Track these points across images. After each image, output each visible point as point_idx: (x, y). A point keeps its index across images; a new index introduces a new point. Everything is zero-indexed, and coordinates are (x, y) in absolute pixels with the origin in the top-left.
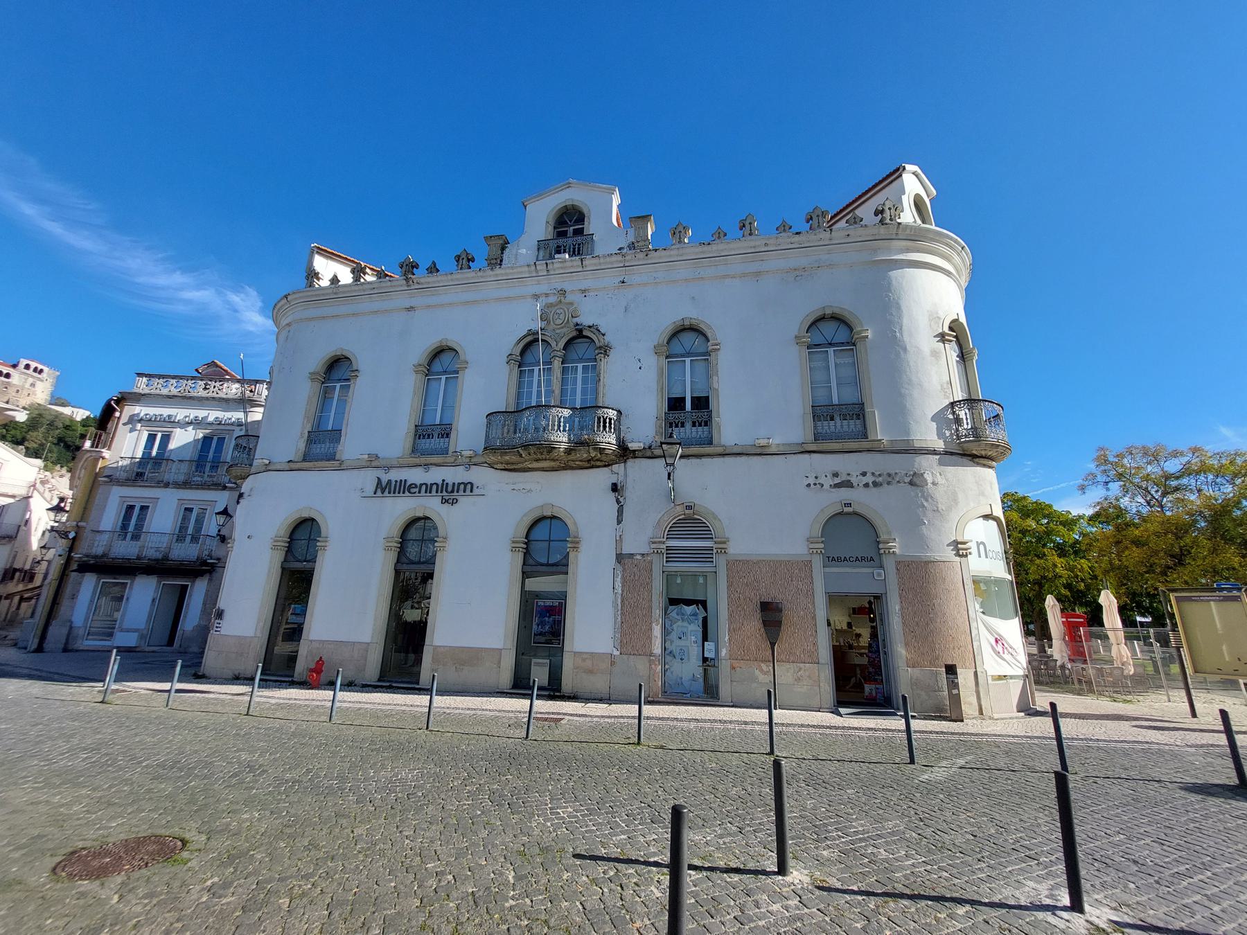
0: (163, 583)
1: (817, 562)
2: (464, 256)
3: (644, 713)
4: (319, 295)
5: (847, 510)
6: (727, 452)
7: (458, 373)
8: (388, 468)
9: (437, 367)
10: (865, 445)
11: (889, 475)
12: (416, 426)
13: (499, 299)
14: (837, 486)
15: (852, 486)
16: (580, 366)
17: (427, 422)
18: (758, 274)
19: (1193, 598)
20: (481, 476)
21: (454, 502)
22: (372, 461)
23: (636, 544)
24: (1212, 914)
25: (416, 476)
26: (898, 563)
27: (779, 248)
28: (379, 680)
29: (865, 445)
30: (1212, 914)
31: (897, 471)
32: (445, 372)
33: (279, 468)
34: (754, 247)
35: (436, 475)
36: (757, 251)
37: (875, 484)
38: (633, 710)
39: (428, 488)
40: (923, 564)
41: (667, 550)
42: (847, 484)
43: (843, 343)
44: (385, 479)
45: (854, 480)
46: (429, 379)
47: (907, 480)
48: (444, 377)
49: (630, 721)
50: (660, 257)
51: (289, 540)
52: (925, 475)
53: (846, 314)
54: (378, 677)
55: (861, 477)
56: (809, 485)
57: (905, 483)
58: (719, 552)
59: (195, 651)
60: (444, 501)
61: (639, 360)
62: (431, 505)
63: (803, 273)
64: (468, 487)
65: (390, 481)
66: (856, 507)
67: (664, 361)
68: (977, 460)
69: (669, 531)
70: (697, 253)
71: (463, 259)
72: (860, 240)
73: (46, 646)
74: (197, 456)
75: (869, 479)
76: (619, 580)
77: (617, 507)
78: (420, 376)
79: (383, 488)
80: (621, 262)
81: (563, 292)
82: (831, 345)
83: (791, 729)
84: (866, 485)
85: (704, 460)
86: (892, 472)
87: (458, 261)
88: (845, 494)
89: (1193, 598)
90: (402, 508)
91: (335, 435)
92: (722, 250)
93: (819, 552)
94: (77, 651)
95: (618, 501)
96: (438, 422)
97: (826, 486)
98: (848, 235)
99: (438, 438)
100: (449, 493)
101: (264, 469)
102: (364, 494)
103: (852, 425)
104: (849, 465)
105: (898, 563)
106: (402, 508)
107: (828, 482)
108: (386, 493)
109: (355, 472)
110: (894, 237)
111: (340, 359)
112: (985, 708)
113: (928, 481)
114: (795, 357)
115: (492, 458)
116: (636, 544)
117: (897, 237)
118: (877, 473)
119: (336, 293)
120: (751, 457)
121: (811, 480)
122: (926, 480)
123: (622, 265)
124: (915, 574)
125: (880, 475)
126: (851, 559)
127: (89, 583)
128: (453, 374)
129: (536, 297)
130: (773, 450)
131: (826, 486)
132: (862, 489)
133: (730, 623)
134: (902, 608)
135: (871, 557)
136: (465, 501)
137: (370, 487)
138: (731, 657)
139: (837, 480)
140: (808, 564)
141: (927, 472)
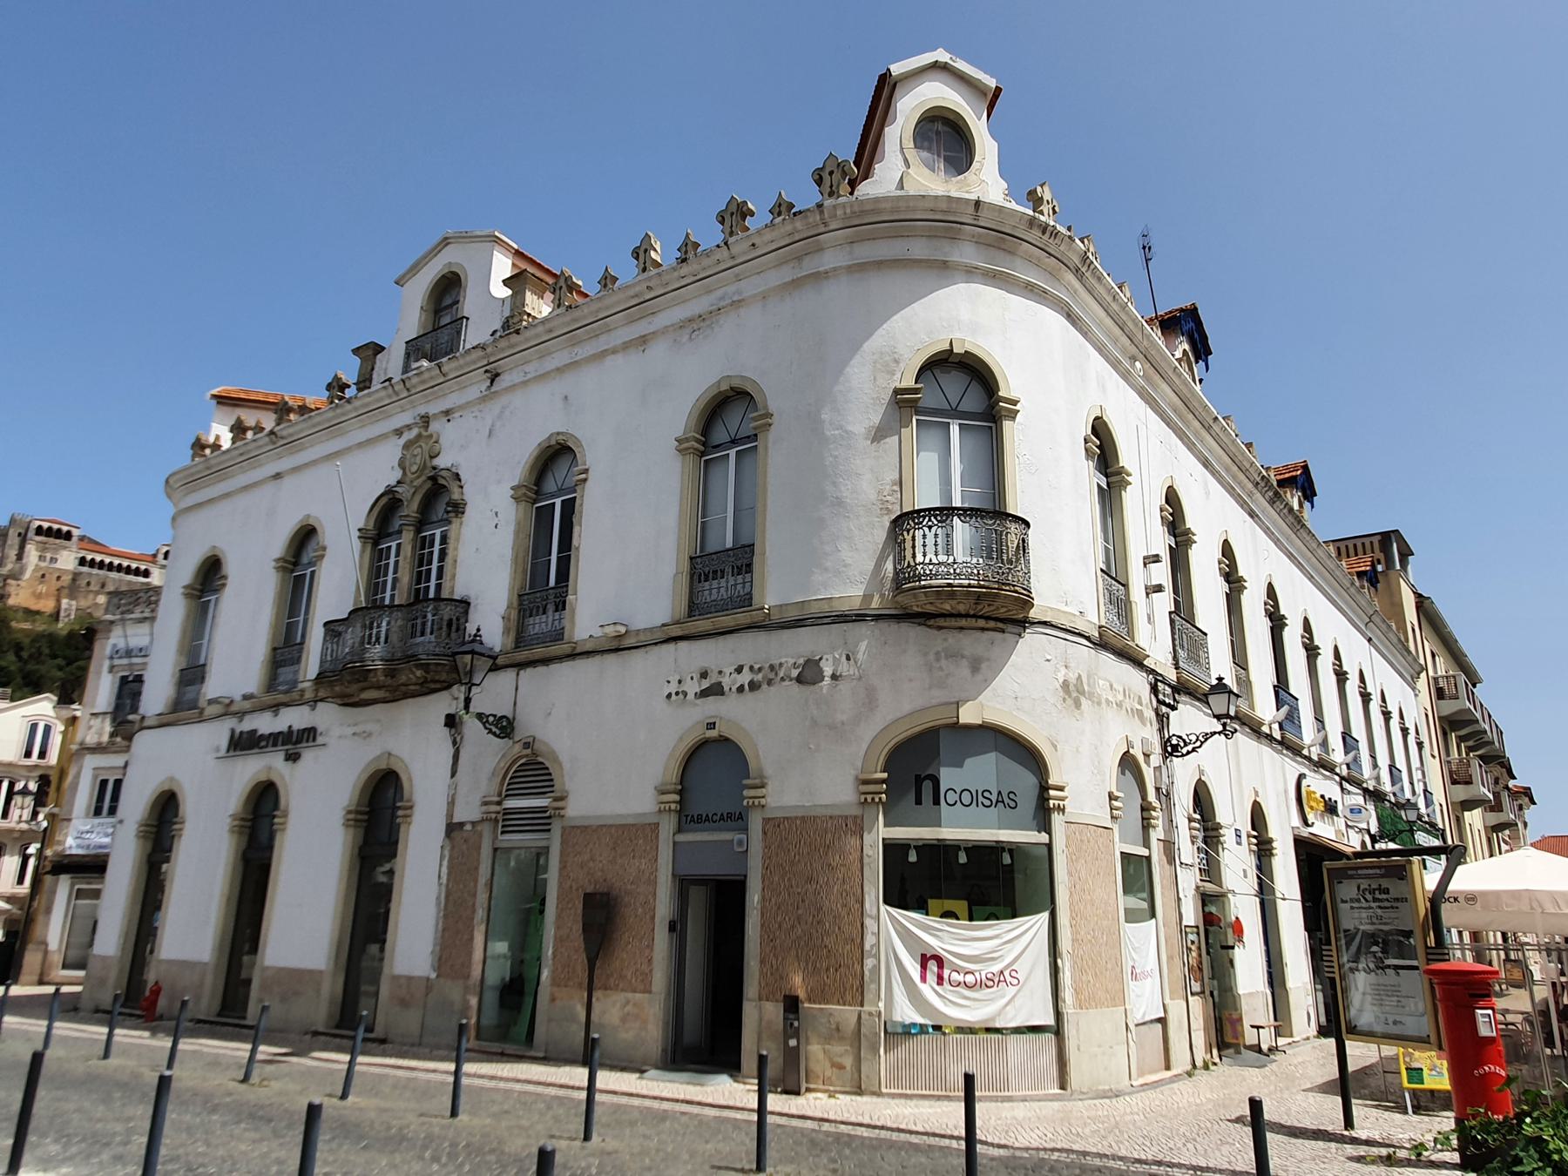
0: (77, 887)
1: (668, 825)
2: (335, 384)
3: (599, 1084)
4: (192, 475)
5: (713, 734)
6: (578, 650)
7: (575, 491)
8: (241, 715)
9: (720, 435)
11: (772, 667)
12: (691, 558)
13: (360, 445)
14: (704, 694)
15: (722, 694)
16: (732, 453)
17: (712, 547)
19: (1350, 872)
20: (326, 716)
22: (227, 709)
23: (468, 811)
26: (766, 821)
27: (669, 289)
28: (219, 1015)
29: (742, 618)
31: (783, 660)
32: (734, 442)
34: (637, 296)
36: (642, 300)
37: (754, 686)
38: (580, 1075)
40: (798, 822)
41: (504, 814)
42: (716, 690)
43: (749, 437)
45: (726, 682)
46: (706, 461)
47: (795, 673)
48: (732, 453)
49: (954, 1144)
50: (527, 340)
51: (368, 809)
52: (822, 664)
54: (218, 1009)
55: (735, 675)
56: (669, 696)
57: (791, 680)
58: (869, 800)
61: (496, 514)
62: (270, 763)
63: (702, 324)
66: (722, 729)
68: (931, 622)
69: (509, 784)
70: (568, 324)
71: (831, 173)
72: (774, 248)
73: (1387, 1075)
74: (113, 705)
75: (745, 677)
76: (445, 863)
77: (452, 751)
78: (690, 459)
80: (484, 358)
83: (1111, 1163)
84: (741, 689)
85: (554, 667)
86: (776, 662)
87: (637, 258)
88: (712, 706)
89: (1350, 872)
91: (742, 559)
92: (597, 311)
93: (877, 800)
95: (454, 743)
96: (729, 544)
97: (691, 696)
98: (753, 245)
99: (700, 582)
102: (220, 755)
104: (719, 655)
105: (766, 821)
106: (251, 768)
107: (693, 688)
110: (822, 229)
111: (730, 397)
112: (868, 1077)
113: (825, 674)
116: (468, 811)
117: (827, 229)
118: (756, 667)
119: (208, 468)
120: (605, 656)
121: (673, 688)
122: (821, 671)
123: (486, 363)
124: (786, 839)
125: (760, 669)
126: (714, 819)
127: (63, 887)
128: (748, 443)
129: (399, 432)
131: (691, 696)
132: (734, 695)
133: (558, 928)
134: (763, 898)
135: (740, 813)
136: (309, 756)
137: (224, 742)
138: (555, 982)
139: (706, 684)
140: (655, 827)
141: (825, 657)
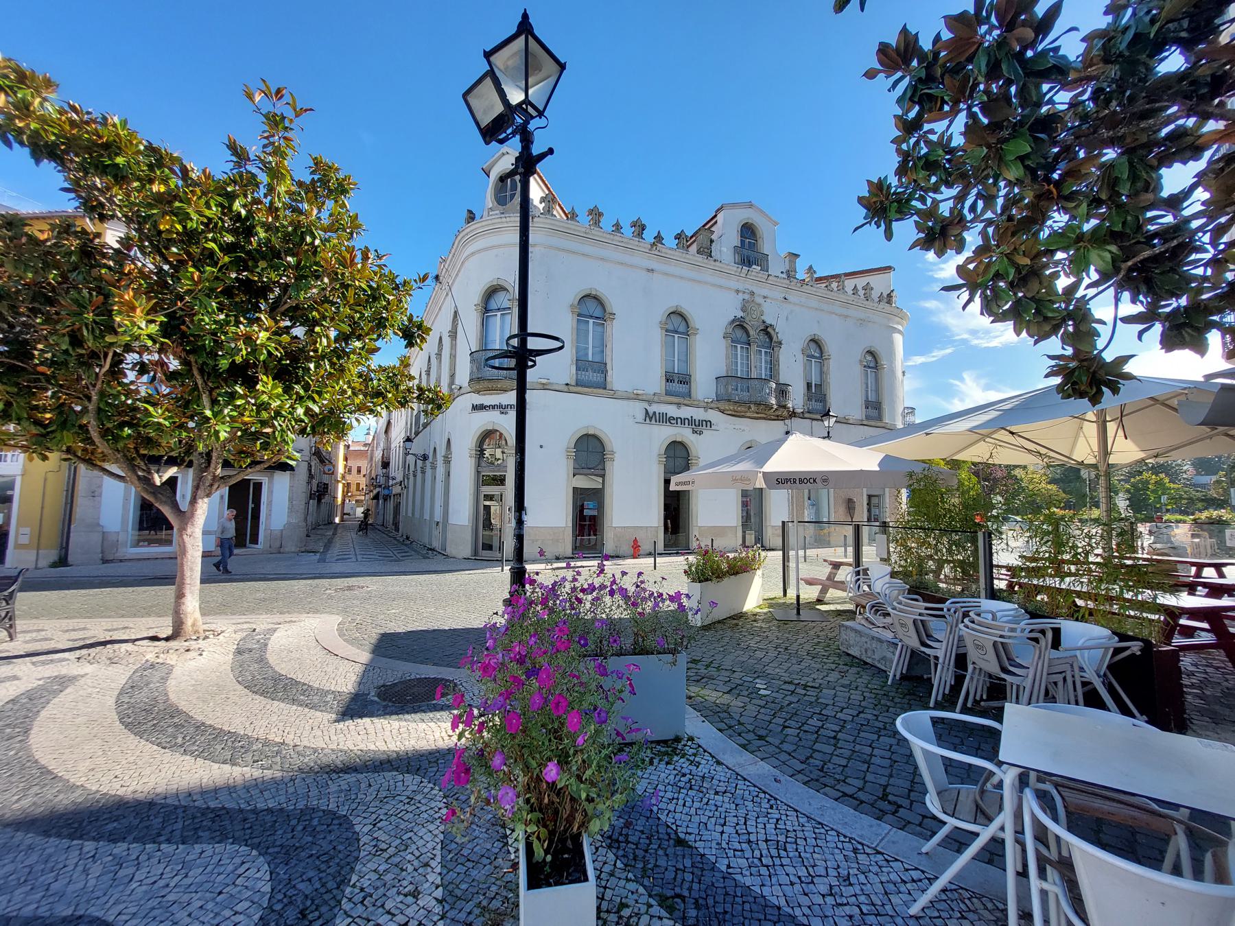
10: (879, 424)
18: (846, 317)
20: (713, 415)
21: (506, 413)
24: (15, 678)
25: (672, 411)
29: (879, 424)
30: (15, 678)
33: (557, 388)
35: (686, 412)
39: (683, 421)
44: (651, 411)
53: (604, 298)
59: (293, 550)
60: (694, 432)
64: (708, 423)
65: (655, 413)
67: (576, 317)
79: (650, 417)
81: (752, 293)
82: (591, 317)
90: (667, 433)
94: (121, 561)
100: (698, 426)
101: (541, 387)
103: (682, 388)
106: (667, 433)
108: (653, 422)
109: (625, 402)
114: (657, 335)
115: (722, 405)
129: (738, 291)
130: (851, 422)
136: (707, 433)
137: (640, 416)
